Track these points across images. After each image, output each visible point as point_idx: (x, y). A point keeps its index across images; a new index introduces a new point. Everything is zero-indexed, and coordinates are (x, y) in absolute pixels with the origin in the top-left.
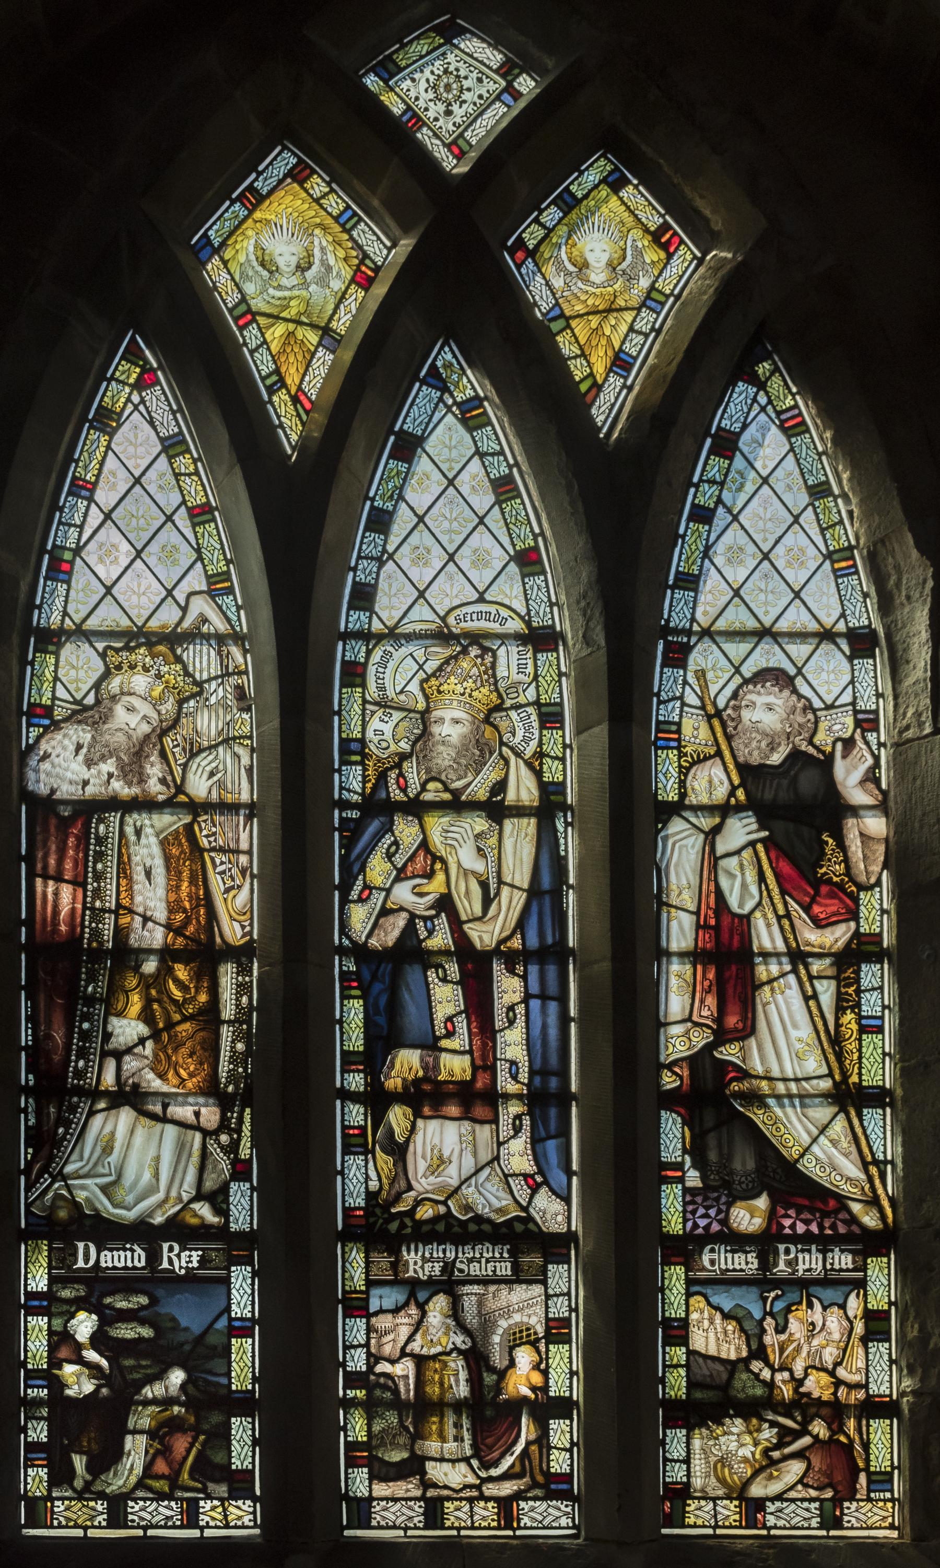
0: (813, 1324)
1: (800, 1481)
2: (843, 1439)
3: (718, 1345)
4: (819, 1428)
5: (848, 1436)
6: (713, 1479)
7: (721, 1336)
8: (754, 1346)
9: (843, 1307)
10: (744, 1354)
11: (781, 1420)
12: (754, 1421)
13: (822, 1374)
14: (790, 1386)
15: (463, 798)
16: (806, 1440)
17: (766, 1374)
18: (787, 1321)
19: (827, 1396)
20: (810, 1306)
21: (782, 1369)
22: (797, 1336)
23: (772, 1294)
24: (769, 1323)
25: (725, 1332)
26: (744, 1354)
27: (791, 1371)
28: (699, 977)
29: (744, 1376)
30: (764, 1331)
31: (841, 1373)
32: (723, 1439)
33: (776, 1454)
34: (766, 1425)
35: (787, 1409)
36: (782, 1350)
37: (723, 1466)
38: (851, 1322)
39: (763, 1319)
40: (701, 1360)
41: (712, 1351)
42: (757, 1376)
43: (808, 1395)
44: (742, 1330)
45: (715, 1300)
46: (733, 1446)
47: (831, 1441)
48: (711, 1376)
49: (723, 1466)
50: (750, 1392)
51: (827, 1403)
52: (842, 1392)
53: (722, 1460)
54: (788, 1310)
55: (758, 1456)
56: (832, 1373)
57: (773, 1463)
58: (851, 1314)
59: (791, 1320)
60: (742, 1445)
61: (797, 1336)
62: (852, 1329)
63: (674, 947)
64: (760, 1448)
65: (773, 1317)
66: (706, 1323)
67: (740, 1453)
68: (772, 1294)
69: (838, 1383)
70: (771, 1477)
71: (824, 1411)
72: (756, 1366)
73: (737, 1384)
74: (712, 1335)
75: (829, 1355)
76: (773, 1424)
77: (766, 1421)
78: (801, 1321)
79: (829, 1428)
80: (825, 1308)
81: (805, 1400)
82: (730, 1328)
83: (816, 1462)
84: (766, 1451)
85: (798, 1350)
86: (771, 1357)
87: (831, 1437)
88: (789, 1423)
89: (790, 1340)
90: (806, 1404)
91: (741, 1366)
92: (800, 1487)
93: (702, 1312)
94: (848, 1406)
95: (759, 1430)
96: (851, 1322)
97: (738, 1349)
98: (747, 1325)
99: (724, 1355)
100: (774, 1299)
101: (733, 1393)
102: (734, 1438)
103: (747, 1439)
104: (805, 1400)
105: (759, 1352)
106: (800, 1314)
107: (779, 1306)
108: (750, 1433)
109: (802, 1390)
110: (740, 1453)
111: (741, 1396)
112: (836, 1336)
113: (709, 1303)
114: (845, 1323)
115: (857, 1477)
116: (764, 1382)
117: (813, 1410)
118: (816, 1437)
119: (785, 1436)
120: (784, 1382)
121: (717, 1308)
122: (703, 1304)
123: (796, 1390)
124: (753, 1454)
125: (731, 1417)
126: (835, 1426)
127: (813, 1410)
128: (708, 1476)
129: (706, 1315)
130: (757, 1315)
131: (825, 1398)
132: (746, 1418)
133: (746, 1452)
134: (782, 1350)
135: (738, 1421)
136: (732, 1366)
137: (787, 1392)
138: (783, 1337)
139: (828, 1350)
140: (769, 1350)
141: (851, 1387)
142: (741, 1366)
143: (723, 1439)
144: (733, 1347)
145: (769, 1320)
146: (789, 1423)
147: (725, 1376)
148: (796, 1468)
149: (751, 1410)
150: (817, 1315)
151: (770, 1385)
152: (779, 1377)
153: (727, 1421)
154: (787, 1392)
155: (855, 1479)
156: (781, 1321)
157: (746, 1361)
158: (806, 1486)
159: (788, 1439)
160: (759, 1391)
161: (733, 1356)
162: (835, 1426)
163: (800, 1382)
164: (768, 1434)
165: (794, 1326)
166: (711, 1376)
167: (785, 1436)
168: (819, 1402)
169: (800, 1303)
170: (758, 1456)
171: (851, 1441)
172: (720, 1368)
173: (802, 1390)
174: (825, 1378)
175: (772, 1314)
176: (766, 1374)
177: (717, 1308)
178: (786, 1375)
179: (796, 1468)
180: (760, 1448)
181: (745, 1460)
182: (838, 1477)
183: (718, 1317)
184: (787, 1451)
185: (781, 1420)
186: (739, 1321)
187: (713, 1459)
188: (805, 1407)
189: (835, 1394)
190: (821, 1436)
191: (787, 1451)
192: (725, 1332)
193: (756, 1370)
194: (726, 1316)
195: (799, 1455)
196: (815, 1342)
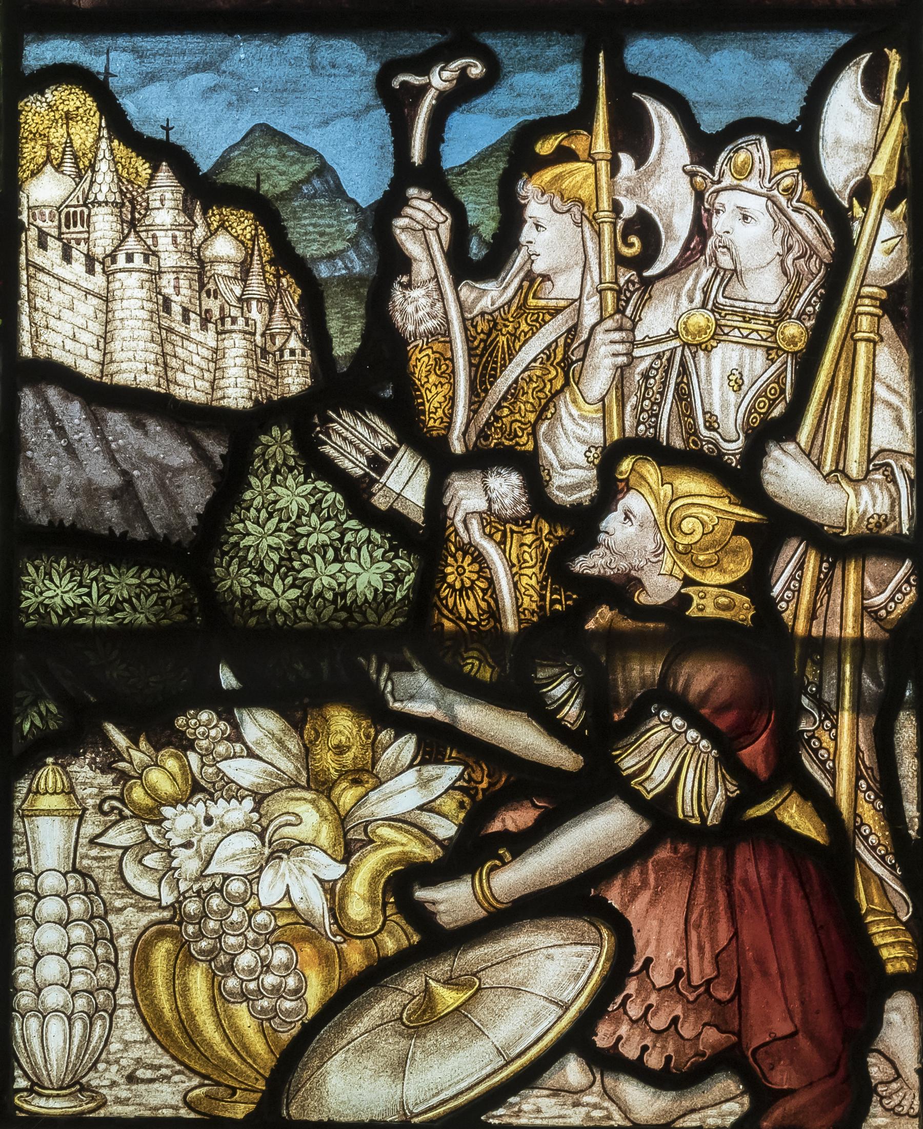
0: (644, 227)
1: (577, 1039)
2: (797, 817)
3: (163, 336)
4: (670, 759)
5: (825, 806)
6: (128, 1027)
7: (182, 294)
8: (345, 344)
9: (799, 138)
10: (295, 380)
11: (475, 717)
12: (343, 723)
13: (691, 484)
14: (530, 545)
15: (511, 625)
16: (607, 827)
17: (405, 483)
18: (512, 216)
19: (715, 597)
20: (632, 136)
21: (481, 460)
22: (565, 286)
23: (440, 79)
24: (422, 227)
25: (201, 269)
26: (295, 380)
27: (530, 467)
28: (653, 505)
29: (293, 494)
30: (393, 264)
31: (790, 475)
32: (181, 821)
33: (453, 901)
34: (406, 747)
35: (511, 669)
36: (486, 364)
37: (184, 957)
38: (837, 218)
39: (393, 203)
40: (73, 413)
41: (133, 367)
42: (357, 494)
43: (619, 590)
44: (286, 258)
45: (148, 108)
46: (235, 853)
47: (736, 829)
48: (126, 491)
49: (184, 957)
50: (324, 576)
51: (714, 636)
52: (795, 572)
53: (174, 923)
54: (520, 155)
55: (358, 909)
56: (742, 478)
57: (437, 940)
58: (838, 172)
59: (536, 209)
60: (282, 850)
61: (565, 286)
62: (844, 251)
63: (686, 669)
64: (371, 863)
65: (445, 196)
66: (104, 226)
67: (270, 891)
68: (440, 79)
69: (774, 527)
70: (423, 1020)
71: (702, 677)
72: (354, 439)
73: (258, 536)
74: (131, 287)
75: (728, 386)
76: (437, 741)
77: (404, 724)
78: (581, 210)
79: (728, 761)
80: (705, 148)
81: (603, 616)
82: (223, 247)
83: (659, 933)
84: (402, 886)
85: (568, 361)
86: (433, 397)
87: (734, 807)
88: (519, 735)
89: (528, 309)
90: (609, 635)
91: (278, 443)
92: (573, 1071)
93: (84, 170)
94: (820, 648)
95: (364, 774)
96: (837, 218)
97: (262, 355)
98: (311, 235)
99: (190, 388)
100: (448, 103)
101: (235, 580)
102: (237, 812)
103: (308, 819)
104: (603, 616)
105: (377, 377)
106: (577, 177)
107: (474, 134)
108: (321, 786)
109: (589, 564)
110: (270, 891)
111: (277, 595)
112: (764, 287)
113: (118, 125)
114: (809, 224)
115: (874, 1023)
116: (391, 523)
117: (642, 671)
118: (659, 811)
119: (504, 802)
120: (494, 521)
121: (162, 152)
122: (87, 131)
123: (557, 568)
124: (335, 893)
125: (226, 705)
126: (754, 754)
127: (642, 671)
128: (102, 1011)
129: (105, 184)
130: (365, 181)
131: (706, 606)
132: (298, 707)
133: (298, 884)
134: (486, 364)
135: (260, 725)
136: (232, 438)
137: (509, 580)
138: (491, 295)
139: (724, 358)
140: (421, 362)
141: (839, 547)
142: (278, 443)
143: (181, 821)
144: (236, 348)
145: (422, 208)
146: (519, 735)
147: (194, 494)
148: (554, 968)
149: (314, 666)
150: (665, 183)
151: (425, 539)
152: (468, 497)
153: (203, 723)
154: (509, 580)
155: (864, 1030)
156: (483, 217)
157: (302, 417)
158: (607, 1062)
159: (517, 819)
160: (369, 573)
161: (237, 393)
162: (754, 754)
163: (581, 526)
164: (413, 797)
165: (551, 239)
166: (126, 491)
167: (504, 802)
168: (678, 629)
169: (581, 119)
170: (358, 909)
171: (841, 833)
172: (164, 447)
173: (589, 564)
174: (704, 504)
175: (435, 180)
176: (405, 483)
177: (162, 152)
178: (506, 486)
179: (554, 968)
180: (371, 863)
181: (294, 927)
182: (772, 1017)
183: (164, 198)
184: (513, 878)
185: (475, 717)
186: (267, 212)
187: (129, 922)
188: (587, 641)
189: (756, 584)
190: (686, 804)
191: (513, 878)
192: (201, 269)
193: (353, 464)
194: (206, 191)
195: (572, 900)
196: (657, 319)
